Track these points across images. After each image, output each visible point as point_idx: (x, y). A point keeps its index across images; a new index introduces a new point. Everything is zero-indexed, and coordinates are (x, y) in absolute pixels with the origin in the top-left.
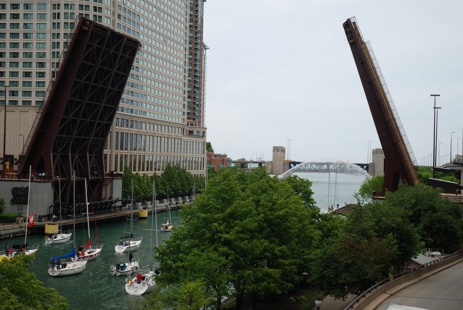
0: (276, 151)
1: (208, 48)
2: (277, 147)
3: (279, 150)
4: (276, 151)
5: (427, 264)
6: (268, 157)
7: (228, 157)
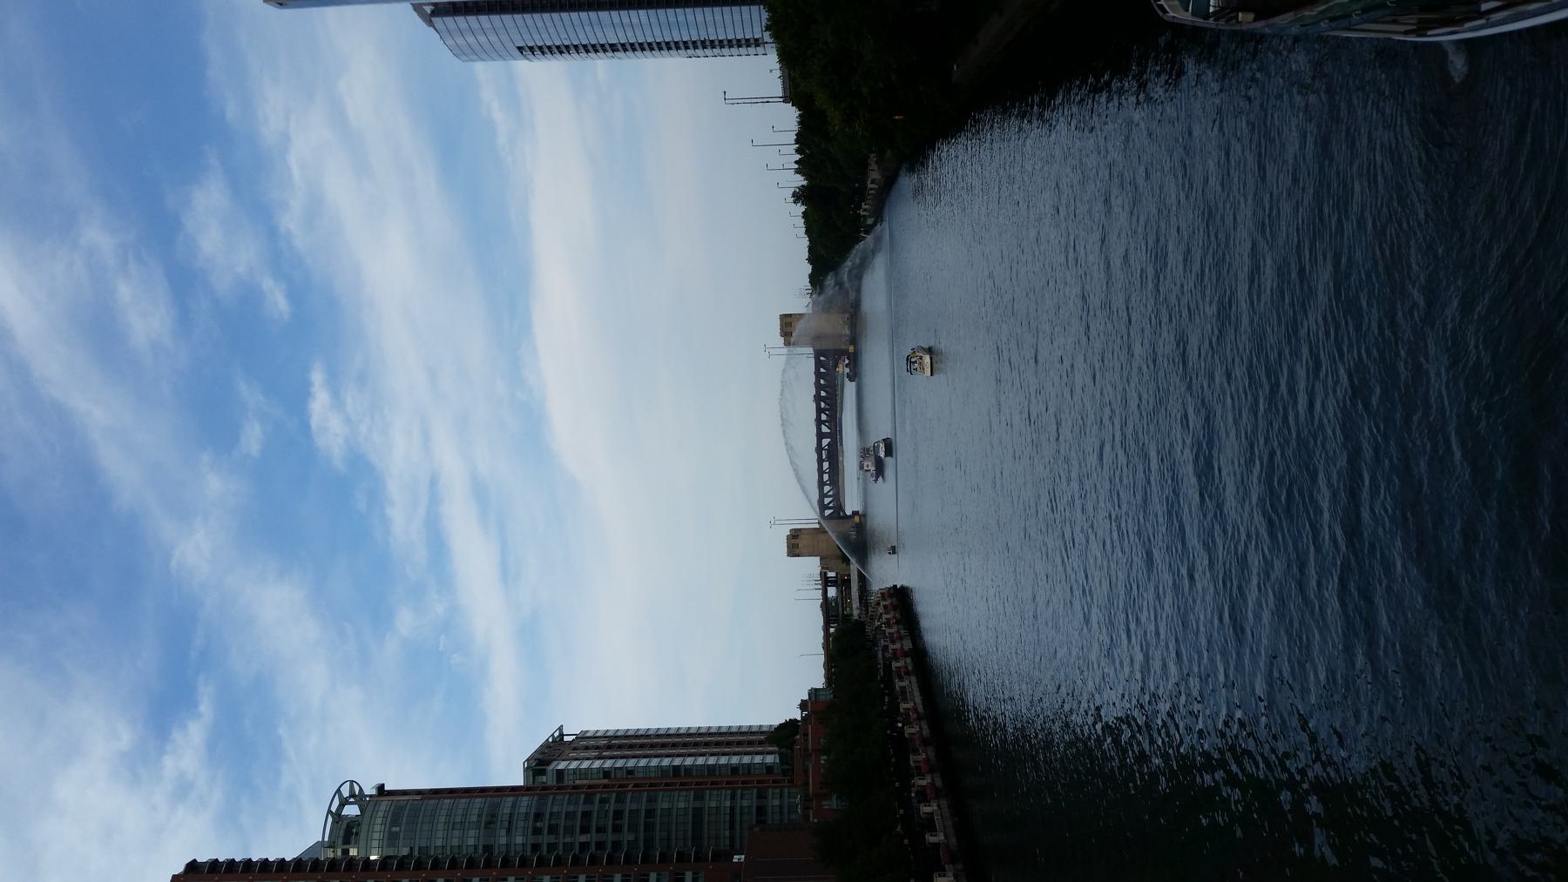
0: (797, 551)
1: (560, 729)
2: (788, 547)
3: (797, 543)
4: (797, 551)
5: (553, 735)
6: (812, 565)
7: (806, 697)
